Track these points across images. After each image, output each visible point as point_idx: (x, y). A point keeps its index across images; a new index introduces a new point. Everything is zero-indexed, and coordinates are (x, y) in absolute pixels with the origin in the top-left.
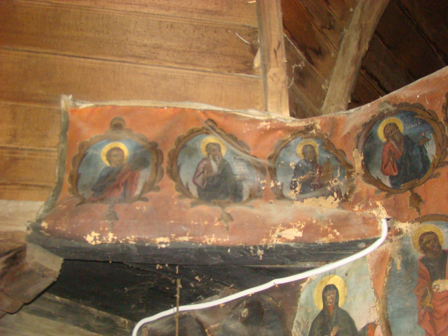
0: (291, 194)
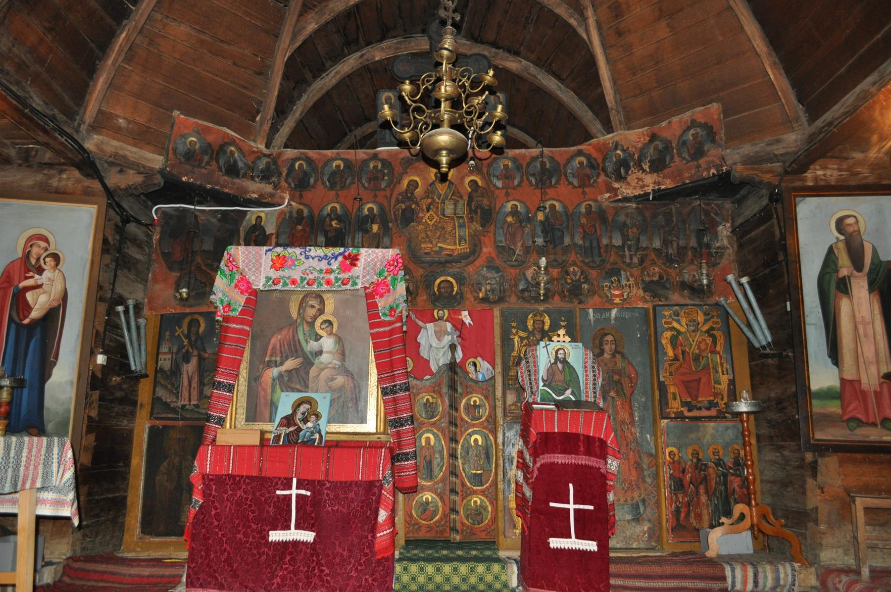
0: (257, 180)
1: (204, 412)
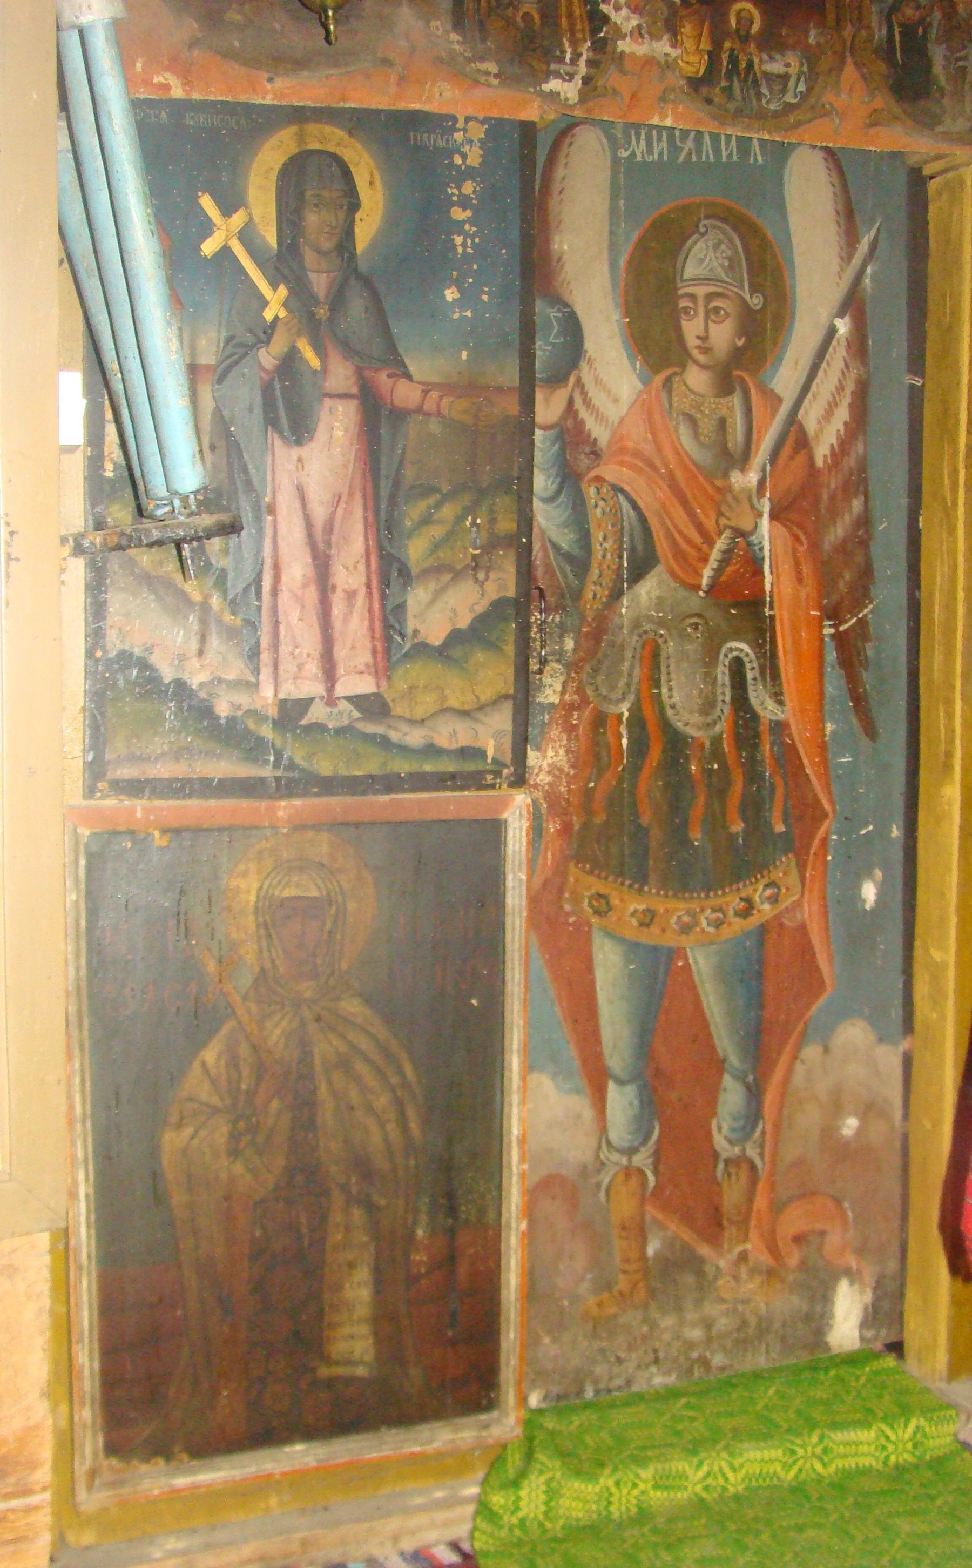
1: (415, 737)
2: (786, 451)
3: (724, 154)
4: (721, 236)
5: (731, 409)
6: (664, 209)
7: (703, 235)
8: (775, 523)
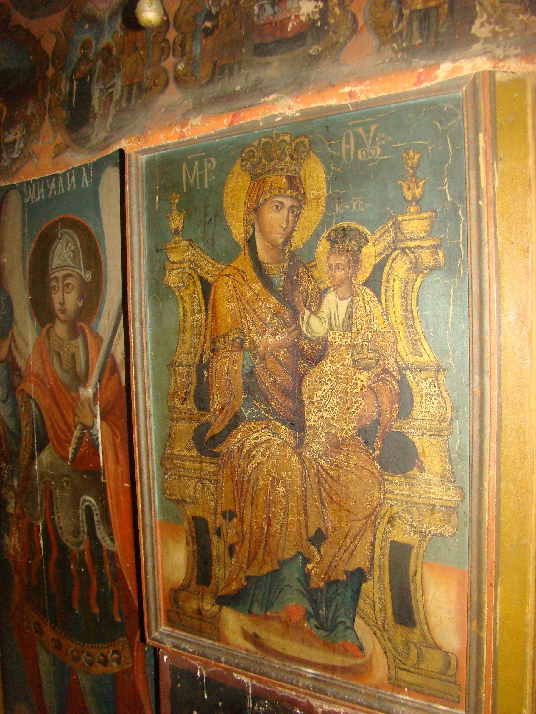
2: (107, 375)
3: (69, 186)
4: (69, 238)
5: (78, 347)
6: (43, 229)
7: (60, 239)
8: (103, 422)
